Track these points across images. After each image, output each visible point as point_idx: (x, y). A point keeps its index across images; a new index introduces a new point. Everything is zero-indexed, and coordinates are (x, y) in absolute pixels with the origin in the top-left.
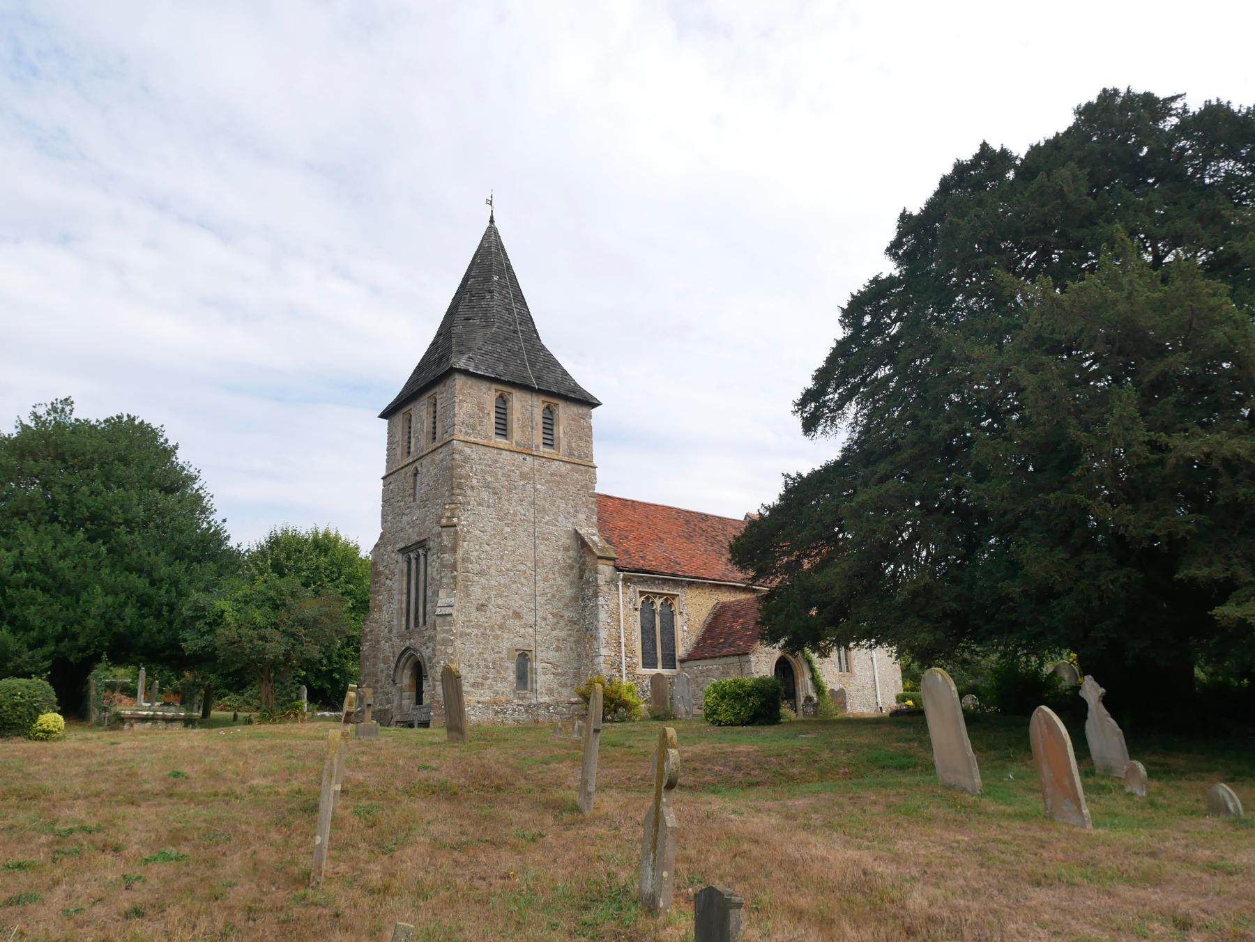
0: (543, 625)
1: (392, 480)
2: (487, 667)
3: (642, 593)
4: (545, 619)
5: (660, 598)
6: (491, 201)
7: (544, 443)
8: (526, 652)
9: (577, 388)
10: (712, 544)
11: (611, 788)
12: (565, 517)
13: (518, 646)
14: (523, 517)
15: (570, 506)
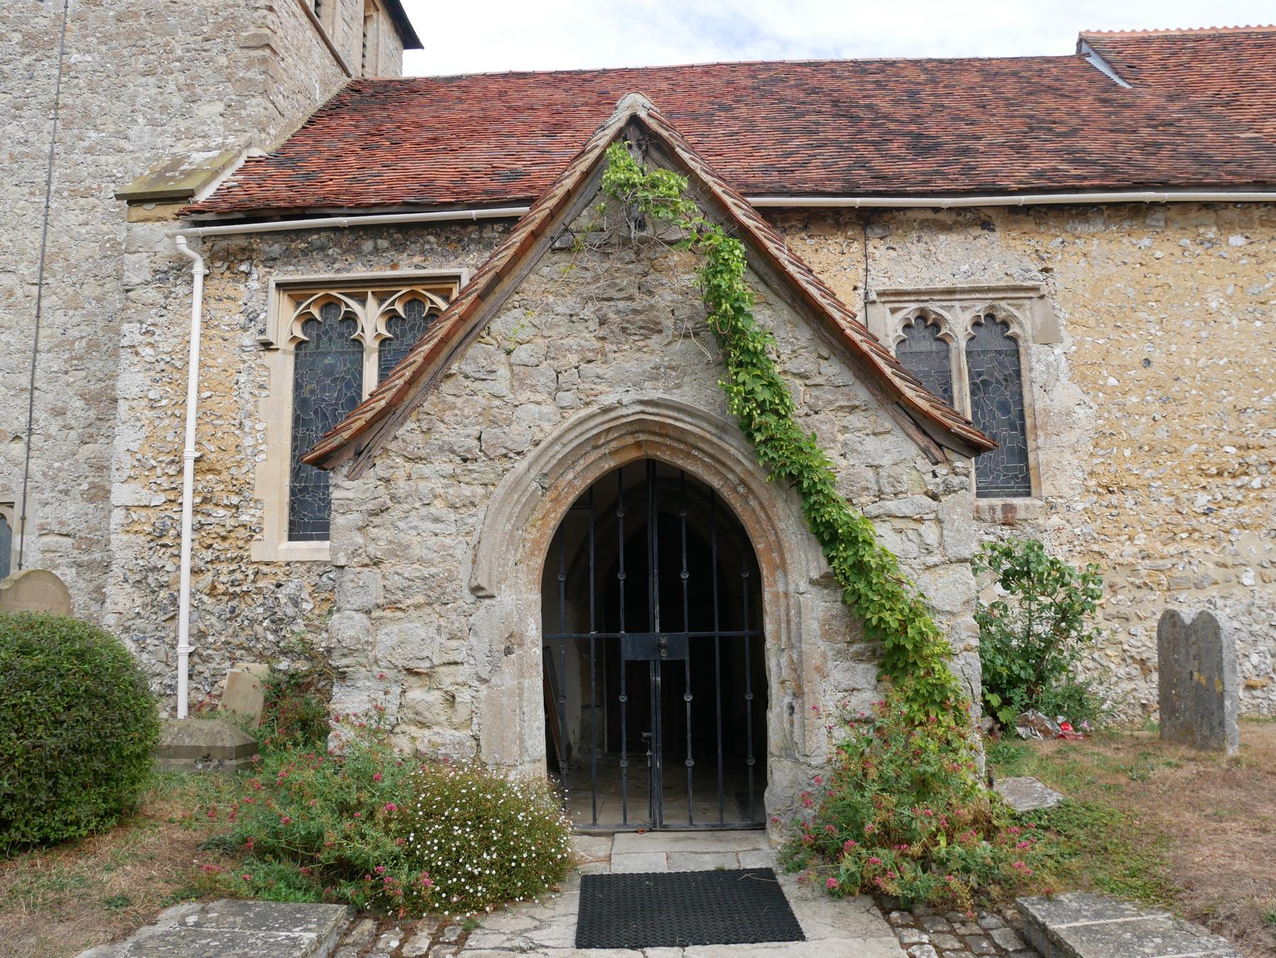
0: (53, 430)
4: (59, 412)
11: (1217, 929)
12: (152, 123)
15: (172, 87)
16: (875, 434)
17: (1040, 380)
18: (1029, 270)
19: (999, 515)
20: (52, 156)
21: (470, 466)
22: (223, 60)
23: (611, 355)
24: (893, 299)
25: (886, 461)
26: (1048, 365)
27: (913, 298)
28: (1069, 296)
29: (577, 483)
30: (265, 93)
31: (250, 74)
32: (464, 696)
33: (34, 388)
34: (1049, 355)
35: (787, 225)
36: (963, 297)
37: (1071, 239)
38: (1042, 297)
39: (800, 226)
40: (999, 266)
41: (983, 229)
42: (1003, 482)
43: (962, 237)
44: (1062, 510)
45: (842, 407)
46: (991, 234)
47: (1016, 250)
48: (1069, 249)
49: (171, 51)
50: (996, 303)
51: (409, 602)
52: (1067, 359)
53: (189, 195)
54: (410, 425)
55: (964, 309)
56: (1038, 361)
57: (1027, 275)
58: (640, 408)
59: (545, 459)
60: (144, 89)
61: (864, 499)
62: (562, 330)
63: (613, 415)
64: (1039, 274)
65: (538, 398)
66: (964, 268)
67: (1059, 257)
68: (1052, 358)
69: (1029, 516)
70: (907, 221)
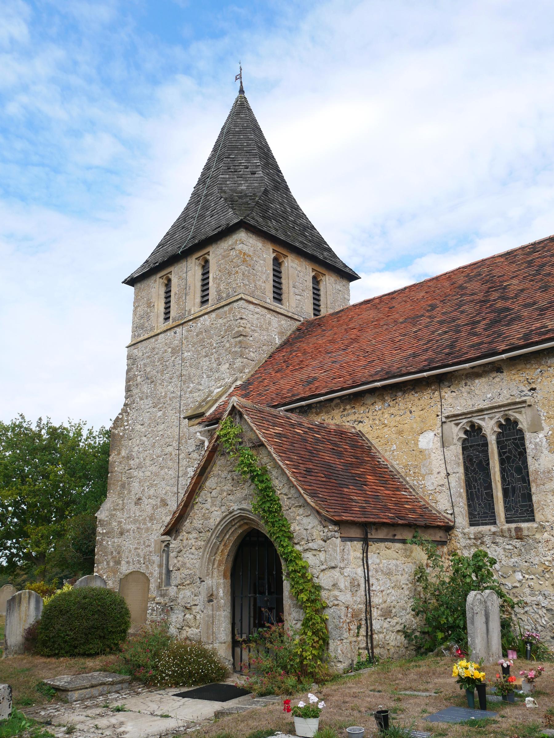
7: (274, 298)
9: (320, 243)
16: (307, 516)
17: (531, 453)
18: (522, 391)
19: (513, 533)
20: (181, 396)
21: (201, 535)
22: (228, 345)
23: (235, 492)
24: (454, 419)
25: (309, 527)
26: (536, 444)
27: (463, 417)
28: (546, 402)
29: (232, 538)
30: (241, 356)
31: (236, 349)
32: (198, 617)
33: (178, 492)
34: (536, 439)
35: (405, 389)
36: (488, 412)
37: (546, 368)
38: (530, 406)
39: (411, 388)
40: (507, 391)
41: (497, 372)
42: (520, 514)
43: (487, 379)
44: (548, 529)
45: (297, 506)
46: (501, 375)
47: (515, 381)
48: (545, 374)
49: (213, 345)
50: (507, 413)
51: (186, 583)
52: (547, 440)
53: (202, 414)
54: (188, 521)
55: (491, 418)
56: (531, 443)
57: (522, 394)
58: (239, 511)
59: (216, 531)
60: (205, 363)
61: (302, 543)
62: (223, 484)
63: (233, 514)
64: (528, 392)
65: (217, 509)
66: (489, 396)
67: (539, 380)
68: (538, 440)
69: (530, 534)
70: (459, 376)
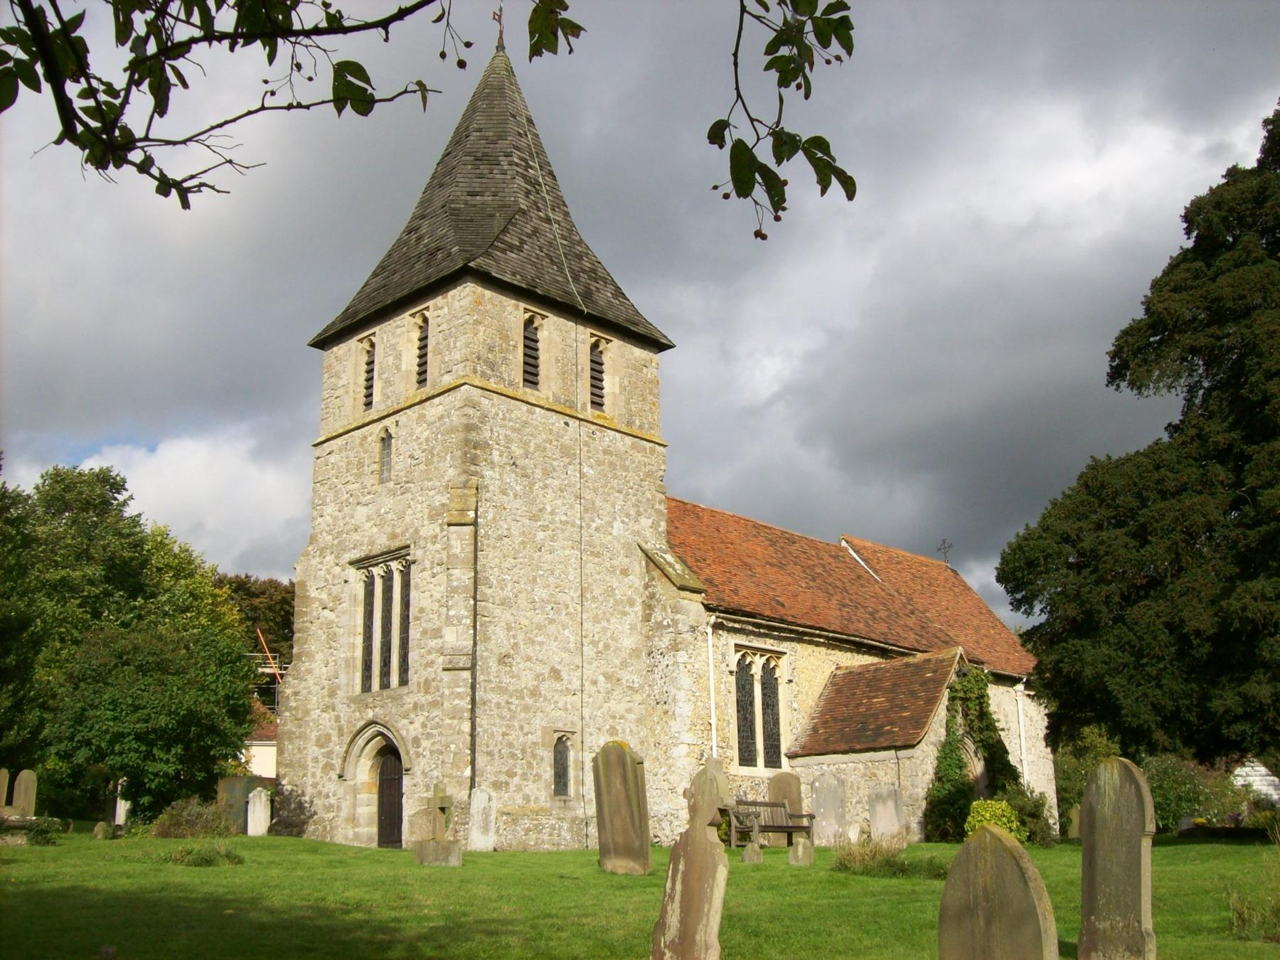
1: (334, 448)
2: (513, 755)
3: (738, 647)
5: (761, 656)
6: (500, 17)
8: (569, 735)
10: (814, 580)
13: (560, 725)
14: (564, 518)
